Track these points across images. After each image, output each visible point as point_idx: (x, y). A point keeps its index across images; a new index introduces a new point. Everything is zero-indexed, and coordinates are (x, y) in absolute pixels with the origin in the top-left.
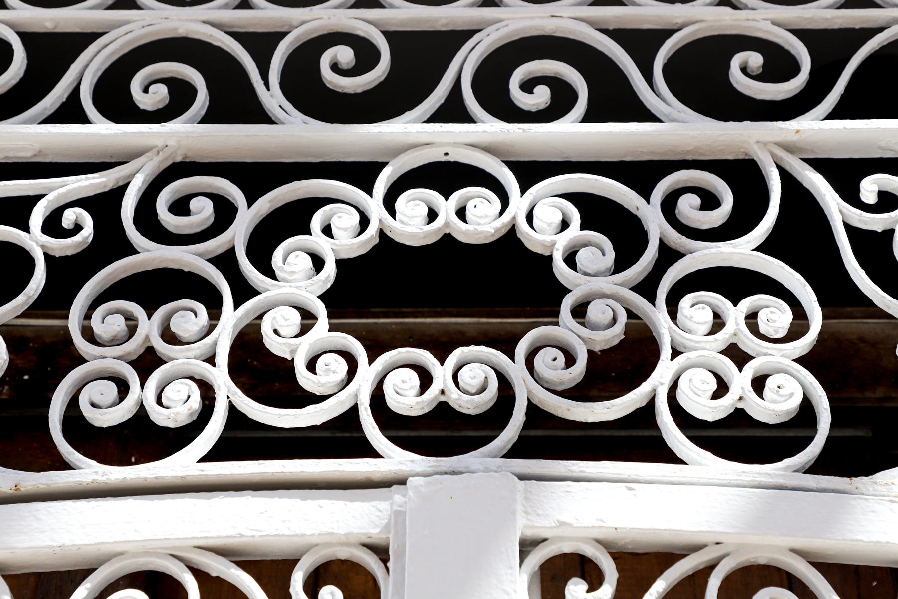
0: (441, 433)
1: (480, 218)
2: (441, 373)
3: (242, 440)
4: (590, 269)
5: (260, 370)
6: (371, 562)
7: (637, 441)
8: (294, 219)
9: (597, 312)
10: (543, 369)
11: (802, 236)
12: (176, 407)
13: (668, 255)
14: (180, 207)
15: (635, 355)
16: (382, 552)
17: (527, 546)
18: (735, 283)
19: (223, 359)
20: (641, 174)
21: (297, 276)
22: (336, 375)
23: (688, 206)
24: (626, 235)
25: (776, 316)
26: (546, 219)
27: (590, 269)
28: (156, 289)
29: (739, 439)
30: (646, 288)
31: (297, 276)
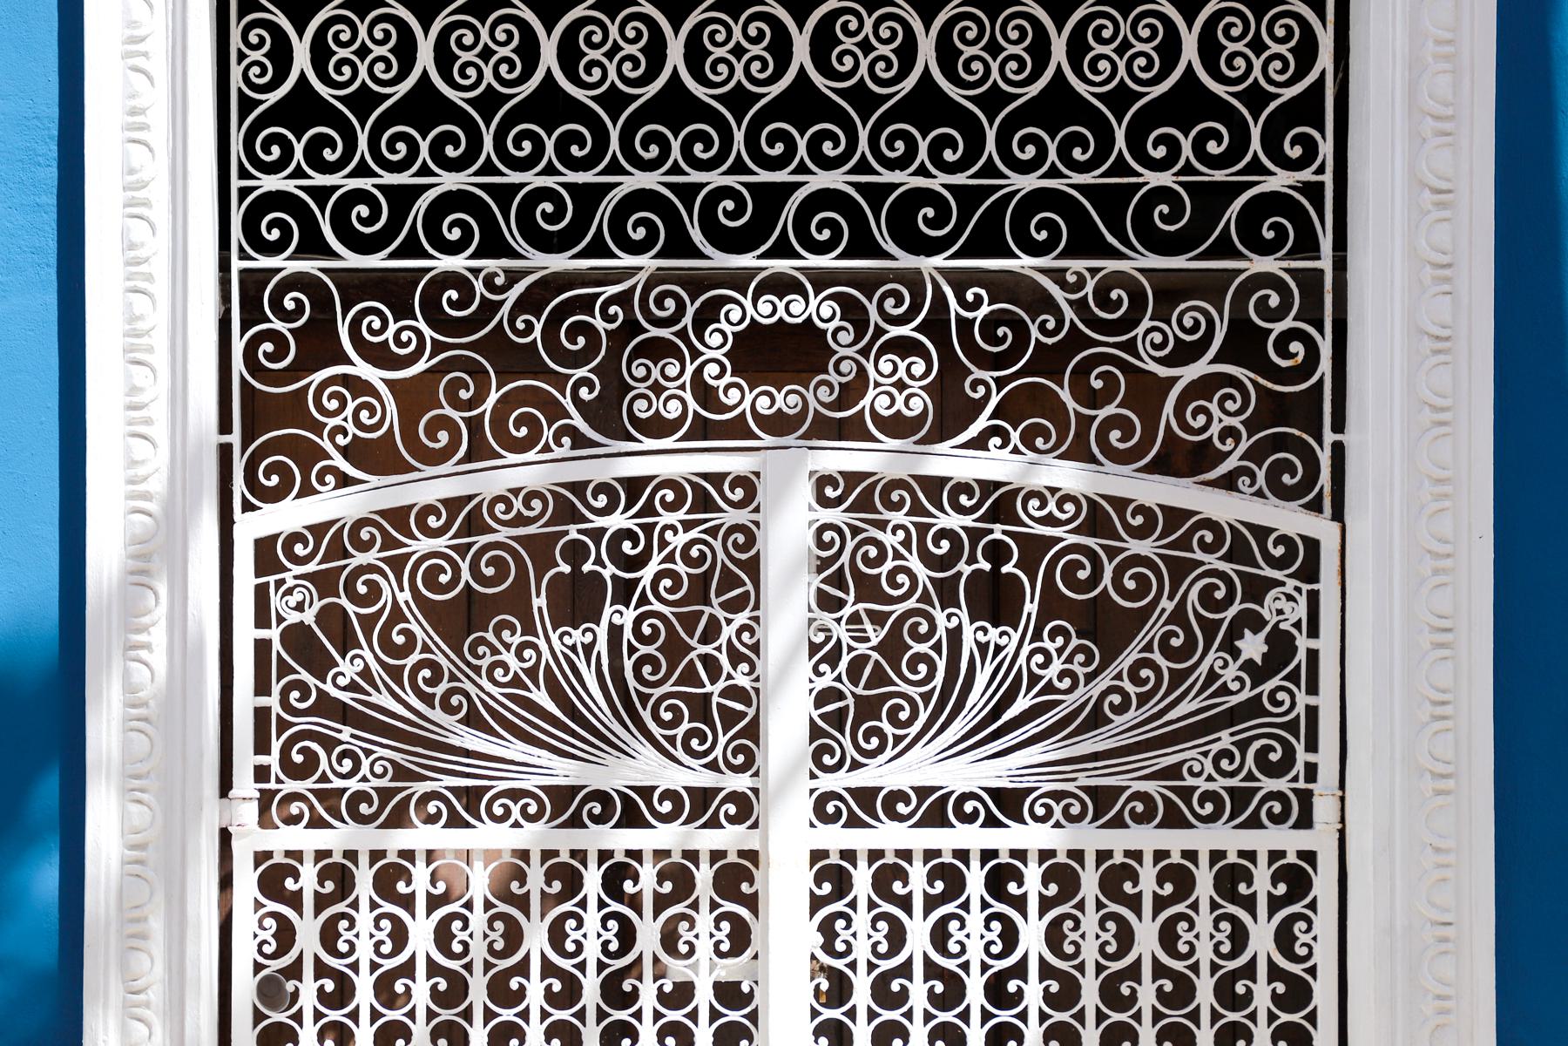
0: (778, 424)
1: (797, 309)
2: (779, 397)
3: (702, 429)
4: (844, 343)
5: (705, 394)
6: (754, 478)
7: (852, 430)
8: (707, 316)
9: (845, 366)
10: (818, 396)
11: (936, 326)
12: (673, 410)
13: (879, 332)
14: (659, 303)
15: (853, 390)
16: (757, 474)
17: (811, 473)
18: (904, 347)
19: (716, 653)
20: (868, 283)
21: (716, 344)
22: (740, 398)
23: (889, 303)
24: (860, 325)
25: (919, 368)
26: (821, 309)
27: (844, 343)
28: (657, 350)
29: (897, 426)
30: (865, 352)
31: (716, 344)
